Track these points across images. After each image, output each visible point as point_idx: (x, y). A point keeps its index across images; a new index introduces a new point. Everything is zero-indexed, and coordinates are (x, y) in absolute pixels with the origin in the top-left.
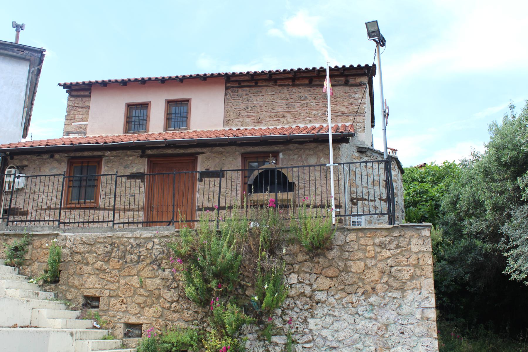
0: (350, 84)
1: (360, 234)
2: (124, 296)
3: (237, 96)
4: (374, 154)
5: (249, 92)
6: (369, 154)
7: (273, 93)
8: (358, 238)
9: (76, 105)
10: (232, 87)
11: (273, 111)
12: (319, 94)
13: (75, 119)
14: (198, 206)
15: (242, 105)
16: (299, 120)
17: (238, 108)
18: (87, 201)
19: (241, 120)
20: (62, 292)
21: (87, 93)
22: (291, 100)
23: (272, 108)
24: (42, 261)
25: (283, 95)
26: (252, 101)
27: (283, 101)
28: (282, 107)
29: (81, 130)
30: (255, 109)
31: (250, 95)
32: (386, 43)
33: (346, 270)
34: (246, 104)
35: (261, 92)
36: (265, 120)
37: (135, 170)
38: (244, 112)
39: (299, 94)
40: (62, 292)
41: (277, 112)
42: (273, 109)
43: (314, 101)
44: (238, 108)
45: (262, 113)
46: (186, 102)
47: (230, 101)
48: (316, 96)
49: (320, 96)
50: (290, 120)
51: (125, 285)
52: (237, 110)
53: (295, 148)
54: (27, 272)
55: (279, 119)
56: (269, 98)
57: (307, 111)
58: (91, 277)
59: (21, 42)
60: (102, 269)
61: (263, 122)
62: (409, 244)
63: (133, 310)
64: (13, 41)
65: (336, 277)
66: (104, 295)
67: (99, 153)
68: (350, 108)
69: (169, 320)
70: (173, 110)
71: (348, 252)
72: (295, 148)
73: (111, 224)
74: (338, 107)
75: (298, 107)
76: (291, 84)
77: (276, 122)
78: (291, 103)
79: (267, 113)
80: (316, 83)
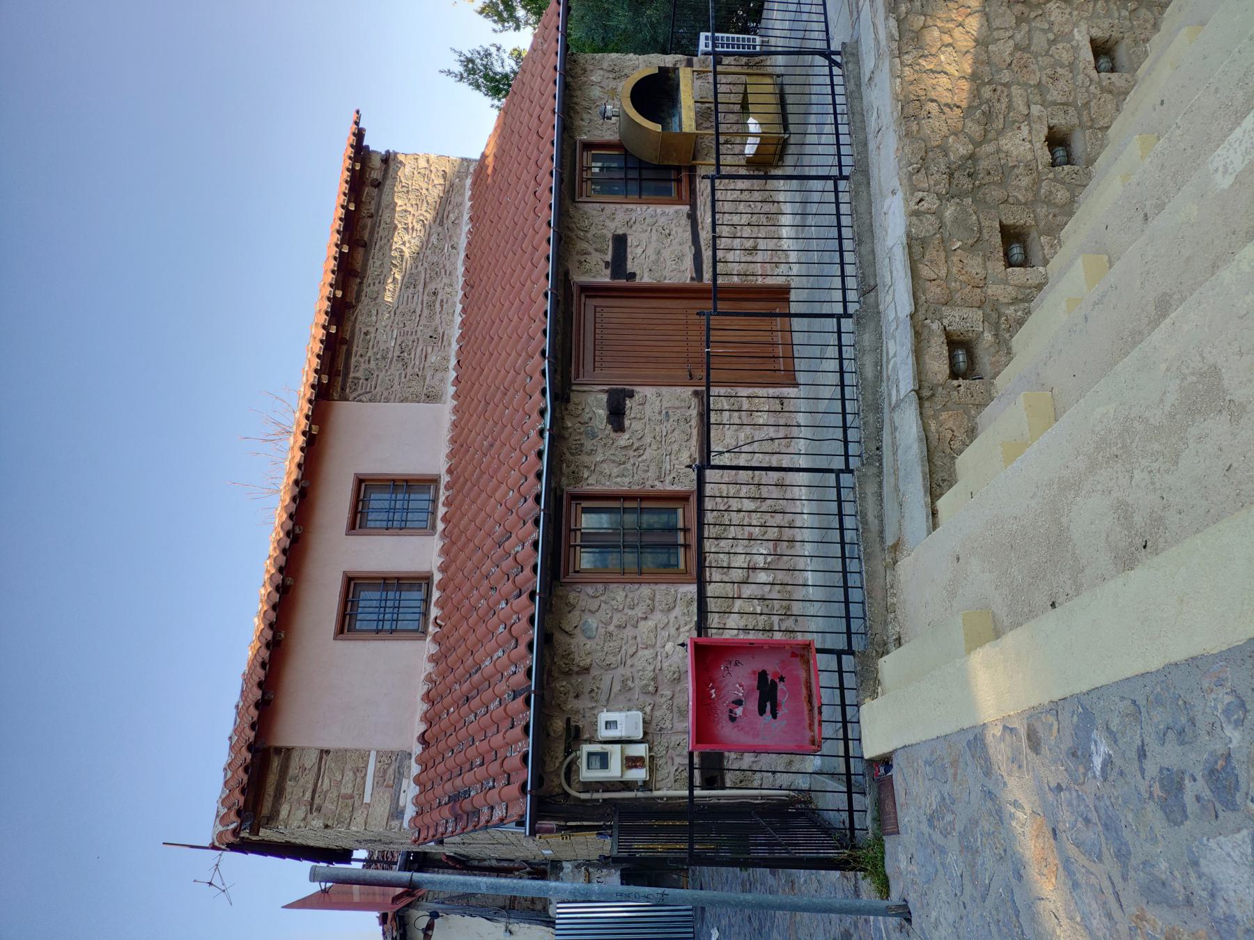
2: (1038, 74)
3: (367, 380)
5: (361, 356)
10: (343, 389)
11: (418, 312)
13: (352, 797)
14: (692, 279)
18: (681, 525)
19: (429, 374)
21: (276, 763)
23: (410, 314)
28: (410, 296)
29: (391, 771)
30: (407, 346)
34: (391, 361)
35: (366, 334)
37: (602, 413)
41: (422, 304)
45: (419, 333)
50: (445, 280)
52: (403, 380)
55: (439, 301)
57: (429, 252)
63: (1065, 53)
73: (842, 185)
76: (358, 280)
77: (445, 306)
78: (406, 280)
79: (420, 324)
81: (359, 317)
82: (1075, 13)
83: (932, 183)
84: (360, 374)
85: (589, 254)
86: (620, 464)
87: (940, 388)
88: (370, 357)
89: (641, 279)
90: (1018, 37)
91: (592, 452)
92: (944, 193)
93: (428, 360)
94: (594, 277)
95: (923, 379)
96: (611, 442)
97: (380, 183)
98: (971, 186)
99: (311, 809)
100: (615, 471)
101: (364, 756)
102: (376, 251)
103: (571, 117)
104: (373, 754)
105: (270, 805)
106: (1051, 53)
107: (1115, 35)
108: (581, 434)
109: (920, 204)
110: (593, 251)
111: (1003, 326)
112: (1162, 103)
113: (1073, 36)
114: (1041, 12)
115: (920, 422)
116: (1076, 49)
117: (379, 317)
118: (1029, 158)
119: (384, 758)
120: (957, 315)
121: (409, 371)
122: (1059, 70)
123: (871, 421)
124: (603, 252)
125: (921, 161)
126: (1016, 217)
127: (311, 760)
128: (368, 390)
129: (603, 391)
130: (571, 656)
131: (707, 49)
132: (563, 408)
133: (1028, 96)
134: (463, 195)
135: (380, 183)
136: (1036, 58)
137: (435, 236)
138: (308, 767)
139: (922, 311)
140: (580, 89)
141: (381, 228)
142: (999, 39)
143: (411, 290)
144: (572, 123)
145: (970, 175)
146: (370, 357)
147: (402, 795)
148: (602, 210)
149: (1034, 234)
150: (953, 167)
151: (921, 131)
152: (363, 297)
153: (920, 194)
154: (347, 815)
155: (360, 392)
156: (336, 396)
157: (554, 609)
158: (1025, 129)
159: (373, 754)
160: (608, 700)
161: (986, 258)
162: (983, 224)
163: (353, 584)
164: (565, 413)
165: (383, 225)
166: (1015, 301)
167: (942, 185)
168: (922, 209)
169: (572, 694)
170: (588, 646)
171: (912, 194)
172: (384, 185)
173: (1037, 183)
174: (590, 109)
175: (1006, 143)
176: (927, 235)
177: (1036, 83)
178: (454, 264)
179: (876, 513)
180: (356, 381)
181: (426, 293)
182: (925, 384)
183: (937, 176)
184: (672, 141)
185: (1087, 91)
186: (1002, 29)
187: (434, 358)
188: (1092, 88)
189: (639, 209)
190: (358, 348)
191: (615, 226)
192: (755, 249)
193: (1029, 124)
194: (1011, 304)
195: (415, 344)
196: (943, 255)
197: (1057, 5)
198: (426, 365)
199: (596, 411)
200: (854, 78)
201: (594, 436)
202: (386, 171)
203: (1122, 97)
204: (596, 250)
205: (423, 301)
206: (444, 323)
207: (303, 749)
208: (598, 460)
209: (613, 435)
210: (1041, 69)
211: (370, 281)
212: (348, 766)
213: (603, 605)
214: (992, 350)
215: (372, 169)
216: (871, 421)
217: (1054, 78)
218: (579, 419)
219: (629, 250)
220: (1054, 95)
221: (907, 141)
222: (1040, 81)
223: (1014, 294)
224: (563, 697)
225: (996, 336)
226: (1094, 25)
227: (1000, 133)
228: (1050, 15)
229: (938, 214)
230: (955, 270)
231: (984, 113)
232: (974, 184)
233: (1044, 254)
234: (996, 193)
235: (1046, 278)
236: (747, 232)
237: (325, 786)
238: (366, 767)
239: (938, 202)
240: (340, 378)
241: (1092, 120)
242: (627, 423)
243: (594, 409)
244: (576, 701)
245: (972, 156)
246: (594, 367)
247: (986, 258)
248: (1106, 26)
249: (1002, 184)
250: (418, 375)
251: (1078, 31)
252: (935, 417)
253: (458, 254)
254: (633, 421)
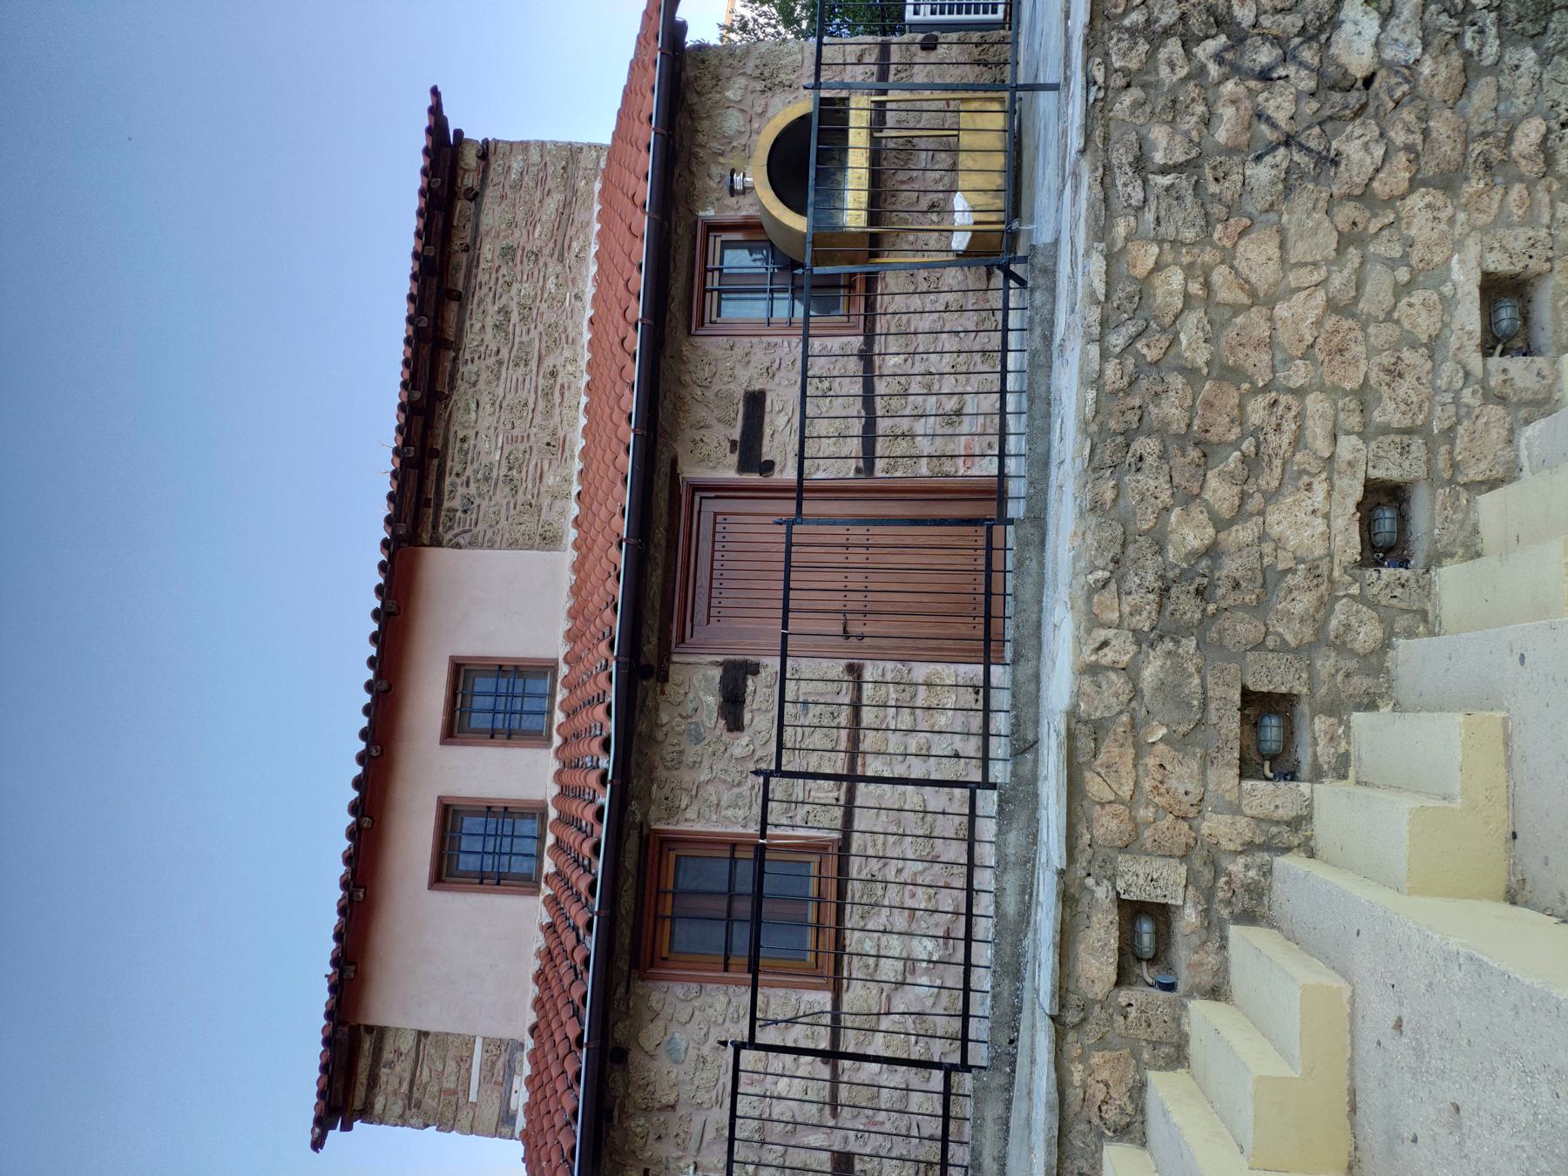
0: (477, 189)
2: (1363, 367)
3: (465, 512)
5: (458, 475)
7: (473, 406)
10: (435, 527)
11: (531, 405)
12: (497, 271)
13: (455, 1093)
15: (498, 497)
16: (570, 329)
17: (508, 510)
19: (546, 502)
20: (1348, 675)
21: (367, 1044)
22: (504, 353)
23: (520, 408)
24: (1196, 791)
25: (484, 376)
26: (490, 467)
27: (504, 375)
28: (521, 379)
29: (500, 1064)
30: (517, 459)
34: (496, 484)
35: (463, 440)
36: (556, 428)
37: (712, 701)
38: (520, 493)
39: (489, 330)
40: (1348, 675)
41: (536, 392)
42: (526, 404)
43: (515, 286)
44: (508, 510)
45: (532, 438)
47: (482, 533)
48: (501, 281)
49: (504, 270)
50: (567, 353)
51: (1314, 361)
52: (512, 512)
53: (686, 173)
54: (1252, 873)
55: (558, 387)
56: (487, 420)
57: (544, 306)
58: (1275, 531)
60: (1241, 473)
61: (561, 434)
66: (1362, 456)
67: (632, 845)
68: (550, 184)
69: (1465, 155)
70: (468, 863)
72: (686, 173)
74: (544, 218)
75: (528, 332)
77: (567, 395)
78: (514, 353)
79: (534, 423)
81: (455, 414)
82: (1461, 216)
83: (1126, 609)
84: (457, 503)
85: (707, 427)
86: (733, 786)
87: (1097, 1008)
88: (468, 478)
89: (781, 471)
90: (1337, 281)
91: (695, 765)
92: (1146, 629)
93: (545, 480)
94: (714, 468)
95: (1072, 987)
96: (722, 749)
97: (477, 194)
98: (1198, 616)
99: (409, 1104)
100: (726, 797)
101: (469, 1042)
102: (475, 306)
103: (692, 173)
104: (479, 1041)
105: (363, 1094)
106: (1396, 315)
107: (1536, 265)
108: (680, 734)
109: (1101, 653)
110: (714, 422)
111: (1221, 895)
112: (1399, 1025)
113: (1449, 269)
114: (1392, 217)
115: (1053, 1075)
116: (1448, 303)
117: (481, 413)
118: (1316, 554)
119: (492, 1047)
120: (1141, 872)
121: (520, 498)
122: (1407, 354)
123: (1006, 994)
124: (730, 424)
125: (1111, 566)
126: (1272, 677)
127: (407, 1044)
128: (467, 527)
129: (717, 664)
130: (651, 1088)
131: (917, 17)
132: (658, 689)
133: (1336, 416)
134: (590, 208)
135: (477, 194)
136: (1364, 329)
138: (405, 1051)
139: (1082, 862)
140: (709, 117)
141: (480, 269)
142: (1299, 289)
143: (521, 370)
144: (693, 183)
145: (1199, 592)
146: (468, 478)
147: (514, 1096)
148: (732, 348)
149: (1304, 708)
150: (1171, 575)
151: (1121, 502)
152: (459, 382)
153: (1103, 634)
154: (450, 1116)
155: (457, 530)
156: (426, 538)
157: (632, 1012)
158: (1320, 488)
159: (479, 1041)
160: (699, 1149)
161: (1207, 761)
162: (1210, 693)
163: (450, 814)
164: (660, 698)
165: (483, 265)
166: (1250, 847)
167: (1145, 614)
168: (1104, 661)
169: (652, 1136)
170: (673, 1075)
171: (1089, 632)
172: (482, 196)
173: (1326, 605)
174: (722, 155)
175: (1280, 521)
176: (1107, 715)
177: (1356, 385)
178: (577, 326)
179: (996, 1153)
180: (451, 515)
181: (541, 374)
182: (1073, 999)
183: (1135, 599)
184: (828, 241)
185: (1456, 400)
186: (1305, 264)
187: (552, 478)
188: (1467, 393)
189: (786, 344)
190: (453, 464)
191: (747, 378)
192: (959, 413)
193: (1329, 479)
194: (1241, 853)
195: (527, 456)
196: (1131, 751)
197: (1428, 199)
198: (542, 489)
199: (704, 698)
200: (1042, 321)
201: (698, 739)
202: (485, 171)
203: (1523, 413)
204: (719, 420)
205: (537, 387)
206: (565, 422)
207: (398, 1029)
208: (702, 778)
209: (727, 736)
210: (1372, 351)
211: (468, 356)
212: (450, 1055)
213: (697, 1013)
214: (1195, 940)
215: (465, 171)
216: (1006, 994)
217: (1395, 373)
218: (680, 709)
219: (767, 419)
220: (1387, 413)
221: (1092, 520)
222: (1366, 378)
223: (1248, 836)
224: (640, 1142)
225: (1206, 912)
226: (1497, 245)
227: (1271, 497)
228: (1409, 224)
229: (1130, 672)
230: (1147, 785)
231: (1245, 458)
232: (1204, 610)
233: (1315, 753)
234: (1244, 629)
235: (1310, 806)
236: (948, 384)
237: (425, 1077)
238: (471, 1057)
239: (1133, 649)
240: (431, 511)
241: (1454, 466)
242: (747, 717)
243: (701, 693)
244: (658, 1145)
245: (1212, 551)
246: (709, 616)
247: (1207, 761)
248: (1519, 245)
249: (1260, 608)
250: (531, 505)
251: (1460, 261)
252: (1083, 1058)
253: (584, 308)
254: (756, 714)
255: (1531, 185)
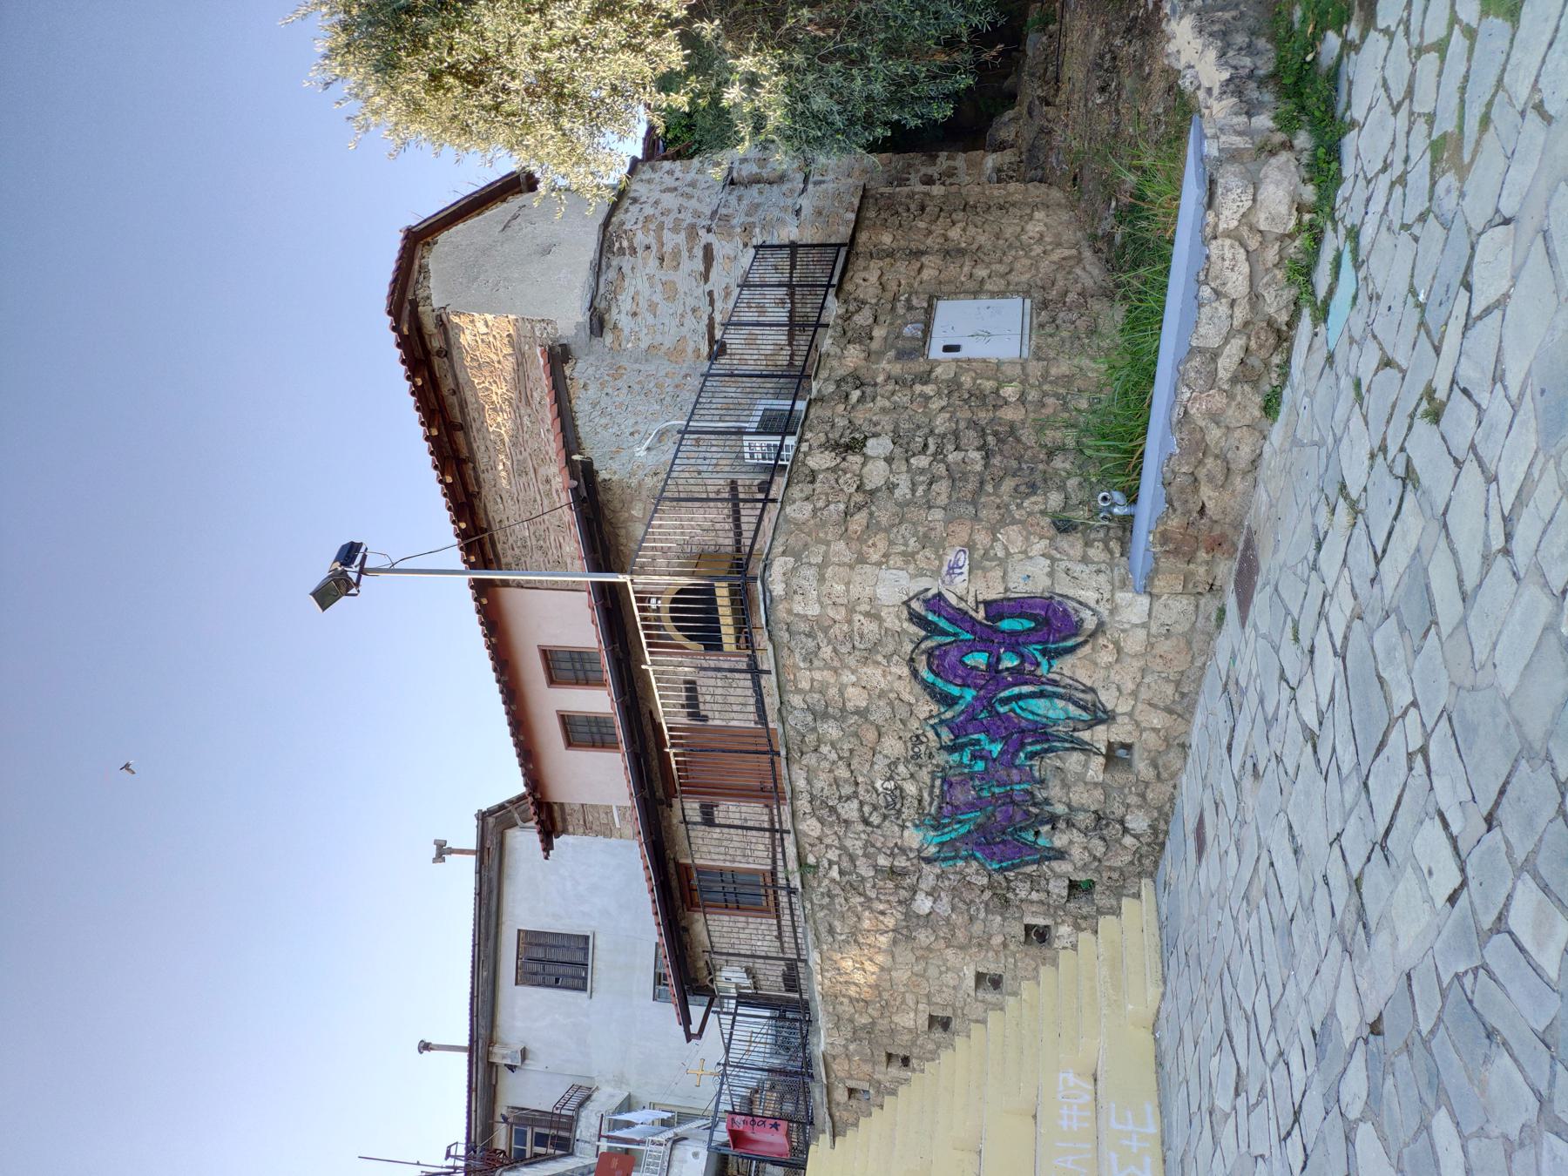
1: (790, 687)
4: (601, 291)
6: (603, 305)
8: (799, 691)
9: (582, 822)
31: (511, 541)
32: (357, 541)
33: (862, 713)
46: (548, 655)
59: (472, 844)
62: (805, 618)
64: (473, 858)
65: (878, 728)
71: (827, 707)
80: (458, 415)
137: (526, 419)
255: (997, 953)
